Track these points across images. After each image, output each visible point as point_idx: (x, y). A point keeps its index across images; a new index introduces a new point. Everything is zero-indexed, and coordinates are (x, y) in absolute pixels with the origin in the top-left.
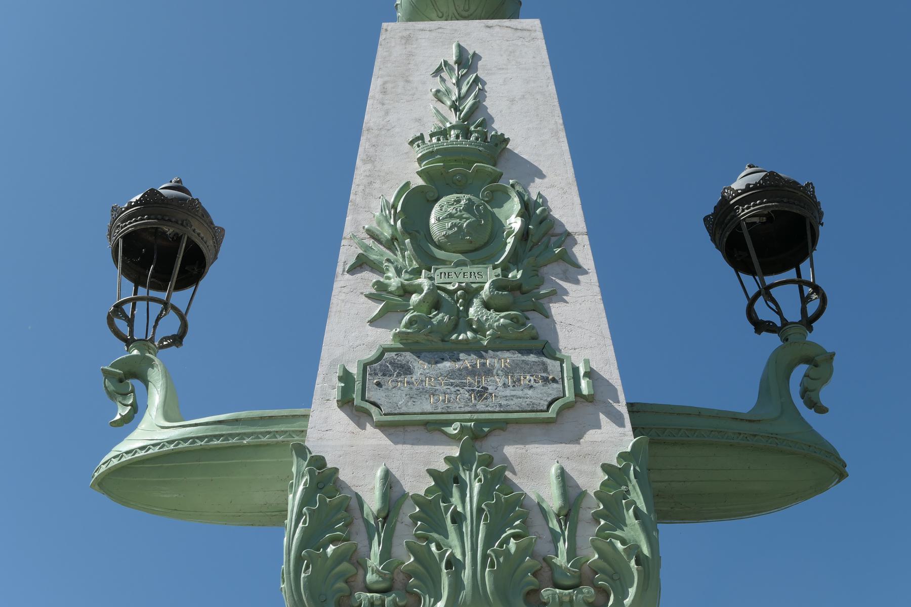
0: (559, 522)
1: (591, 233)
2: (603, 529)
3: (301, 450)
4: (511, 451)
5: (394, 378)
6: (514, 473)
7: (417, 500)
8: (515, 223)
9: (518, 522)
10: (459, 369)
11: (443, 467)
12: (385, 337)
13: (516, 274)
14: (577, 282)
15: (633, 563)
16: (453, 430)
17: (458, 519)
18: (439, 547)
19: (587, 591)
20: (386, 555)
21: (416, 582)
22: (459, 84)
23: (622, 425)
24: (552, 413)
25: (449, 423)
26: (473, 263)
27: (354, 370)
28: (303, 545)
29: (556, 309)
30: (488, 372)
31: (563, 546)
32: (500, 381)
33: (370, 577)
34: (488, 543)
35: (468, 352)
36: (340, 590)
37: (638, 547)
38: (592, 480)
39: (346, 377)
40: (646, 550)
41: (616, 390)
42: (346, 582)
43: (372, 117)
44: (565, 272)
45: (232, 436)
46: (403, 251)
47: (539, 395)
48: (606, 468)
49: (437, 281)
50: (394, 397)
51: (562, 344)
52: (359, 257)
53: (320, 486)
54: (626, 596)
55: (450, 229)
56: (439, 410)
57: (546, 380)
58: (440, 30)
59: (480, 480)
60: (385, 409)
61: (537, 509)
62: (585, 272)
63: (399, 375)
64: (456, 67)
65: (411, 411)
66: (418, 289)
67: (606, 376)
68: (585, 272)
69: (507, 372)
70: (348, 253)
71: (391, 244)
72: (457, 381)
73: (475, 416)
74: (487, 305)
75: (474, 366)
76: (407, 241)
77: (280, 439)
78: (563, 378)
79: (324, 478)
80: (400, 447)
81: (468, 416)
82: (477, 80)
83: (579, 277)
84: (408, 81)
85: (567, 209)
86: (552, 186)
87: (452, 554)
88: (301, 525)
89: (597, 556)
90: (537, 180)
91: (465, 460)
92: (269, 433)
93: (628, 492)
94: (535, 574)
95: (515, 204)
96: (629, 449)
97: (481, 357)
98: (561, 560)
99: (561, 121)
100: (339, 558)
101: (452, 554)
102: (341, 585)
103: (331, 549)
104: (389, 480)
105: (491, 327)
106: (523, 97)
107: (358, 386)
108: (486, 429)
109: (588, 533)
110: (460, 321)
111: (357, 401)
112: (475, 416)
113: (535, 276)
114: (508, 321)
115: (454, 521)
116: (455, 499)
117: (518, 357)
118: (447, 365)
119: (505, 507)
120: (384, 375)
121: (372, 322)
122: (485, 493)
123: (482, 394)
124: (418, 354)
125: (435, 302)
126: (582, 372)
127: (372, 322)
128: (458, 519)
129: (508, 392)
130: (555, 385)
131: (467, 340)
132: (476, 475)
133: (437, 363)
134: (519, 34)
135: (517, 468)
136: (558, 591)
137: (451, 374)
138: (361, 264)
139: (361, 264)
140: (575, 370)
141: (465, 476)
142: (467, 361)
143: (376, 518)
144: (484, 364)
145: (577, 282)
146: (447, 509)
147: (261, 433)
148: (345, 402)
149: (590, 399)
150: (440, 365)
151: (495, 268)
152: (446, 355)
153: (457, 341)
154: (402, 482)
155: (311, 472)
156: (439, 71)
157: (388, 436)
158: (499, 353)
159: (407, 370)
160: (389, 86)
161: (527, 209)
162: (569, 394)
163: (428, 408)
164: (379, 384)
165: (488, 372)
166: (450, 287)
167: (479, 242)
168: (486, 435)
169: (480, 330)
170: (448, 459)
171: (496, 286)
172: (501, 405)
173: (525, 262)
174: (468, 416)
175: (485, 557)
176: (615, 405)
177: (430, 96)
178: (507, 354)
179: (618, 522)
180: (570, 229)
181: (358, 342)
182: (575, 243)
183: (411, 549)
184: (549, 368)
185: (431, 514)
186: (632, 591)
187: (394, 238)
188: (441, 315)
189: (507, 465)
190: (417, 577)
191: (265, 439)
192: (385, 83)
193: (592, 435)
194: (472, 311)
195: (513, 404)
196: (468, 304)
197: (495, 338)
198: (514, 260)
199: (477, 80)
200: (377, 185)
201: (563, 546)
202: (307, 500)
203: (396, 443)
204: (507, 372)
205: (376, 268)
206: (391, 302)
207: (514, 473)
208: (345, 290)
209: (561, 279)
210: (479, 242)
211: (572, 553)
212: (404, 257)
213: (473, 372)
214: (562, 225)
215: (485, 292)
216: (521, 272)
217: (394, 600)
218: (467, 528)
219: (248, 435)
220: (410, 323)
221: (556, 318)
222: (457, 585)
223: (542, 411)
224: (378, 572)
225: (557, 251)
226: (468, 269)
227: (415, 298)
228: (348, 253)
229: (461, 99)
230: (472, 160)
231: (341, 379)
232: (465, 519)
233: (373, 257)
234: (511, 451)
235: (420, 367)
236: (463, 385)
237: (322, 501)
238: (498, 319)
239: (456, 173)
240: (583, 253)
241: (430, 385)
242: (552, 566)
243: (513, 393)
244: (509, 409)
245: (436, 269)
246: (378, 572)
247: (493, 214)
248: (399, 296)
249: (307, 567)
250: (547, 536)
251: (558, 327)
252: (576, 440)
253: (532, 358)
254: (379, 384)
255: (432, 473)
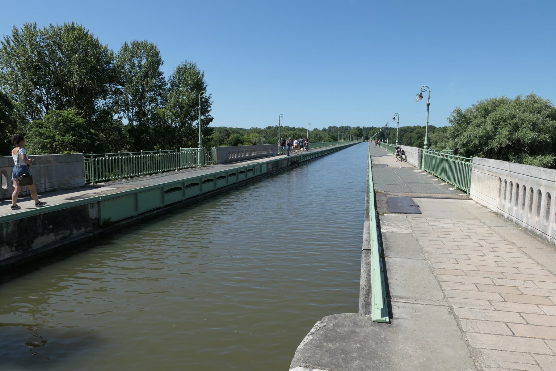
4: (101, 223)
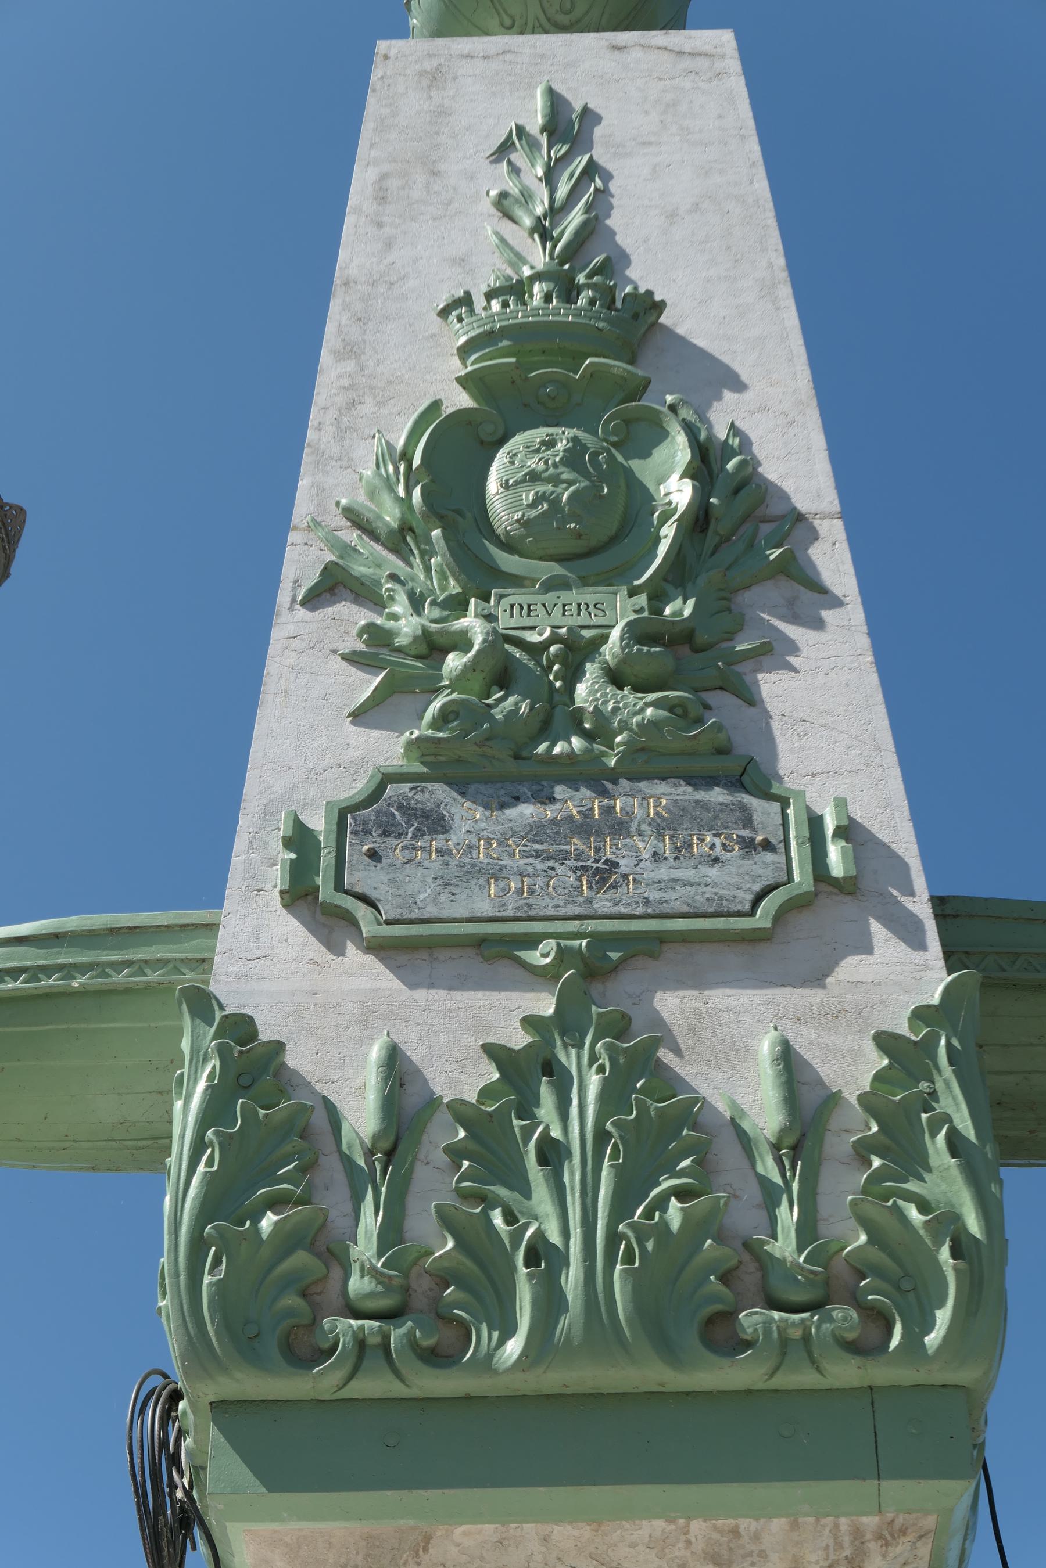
0: (779, 1161)
1: (850, 513)
2: (877, 1177)
3: (201, 1003)
4: (670, 1004)
5: (407, 840)
6: (678, 1052)
7: (460, 1112)
8: (679, 492)
9: (686, 1163)
10: (554, 821)
11: (518, 1039)
12: (388, 748)
13: (681, 608)
14: (818, 624)
15: (945, 1254)
16: (540, 956)
17: (551, 1154)
18: (510, 1218)
19: (843, 1315)
20: (391, 1234)
21: (461, 1295)
22: (550, 178)
23: (920, 945)
24: (762, 919)
25: (532, 941)
26: (585, 582)
27: (318, 822)
28: (206, 1212)
29: (770, 685)
30: (620, 827)
31: (788, 1216)
32: (645, 848)
33: (357, 1285)
34: (621, 1208)
35: (573, 782)
36: (290, 1312)
37: (956, 1218)
38: (852, 1069)
39: (300, 839)
40: (974, 1225)
41: (905, 867)
42: (304, 1294)
43: (354, 255)
44: (791, 602)
45: (47, 970)
46: (426, 555)
47: (733, 877)
48: (885, 1041)
49: (504, 623)
50: (409, 883)
51: (784, 765)
52: (328, 570)
53: (245, 1081)
54: (928, 1326)
55: (533, 505)
56: (510, 913)
57: (749, 845)
58: (508, 57)
59: (601, 1069)
60: (387, 911)
61: (729, 1133)
62: (837, 603)
63: (418, 834)
64: (544, 140)
65: (446, 914)
66: (461, 642)
67: (885, 836)
68: (837, 603)
69: (661, 827)
70: (302, 562)
71: (400, 540)
72: (552, 848)
73: (591, 926)
74: (615, 678)
75: (587, 813)
76: (436, 533)
77: (154, 977)
78: (786, 841)
79: (252, 1066)
80: (421, 994)
81: (573, 926)
82: (592, 169)
83: (825, 614)
84: (435, 173)
85: (797, 463)
86: (763, 409)
87: (540, 1234)
88: (201, 1168)
89: (863, 1238)
90: (728, 396)
91: (567, 1024)
92: (129, 963)
93: (933, 1094)
94: (725, 1278)
95: (678, 450)
96: (936, 1000)
97: (603, 793)
98: (784, 1246)
99: (781, 261)
100: (288, 1240)
101: (540, 1234)
102: (291, 1300)
103: (268, 1222)
104: (397, 1069)
105: (624, 726)
106: (696, 208)
107: (326, 860)
108: (615, 956)
109: (844, 1187)
110: (555, 714)
111: (326, 892)
112: (591, 926)
113: (723, 609)
114: (663, 713)
115: (543, 1160)
116: (547, 1110)
117: (685, 793)
118: (527, 811)
119: (660, 1125)
120: (386, 834)
121: (359, 716)
122: (613, 1096)
123: (605, 875)
124: (461, 786)
125: (499, 671)
126: (830, 825)
127: (359, 716)
128: (551, 1154)
129: (663, 872)
130: (769, 857)
131: (570, 757)
132: (593, 1058)
133: (503, 806)
134: (687, 63)
135: (684, 1042)
136: (776, 1315)
137: (536, 831)
138: (332, 586)
139: (332, 586)
140: (815, 822)
141: (569, 1059)
142: (571, 801)
143: (369, 1153)
144: (609, 810)
145: (818, 624)
146: (527, 1133)
147: (112, 965)
148: (299, 895)
149: (847, 887)
150: (511, 813)
151: (633, 593)
152: (525, 790)
153: (549, 759)
154: (428, 1074)
155: (223, 1052)
156: (504, 149)
157: (396, 969)
158: (643, 785)
159: (436, 823)
160: (393, 183)
161: (705, 463)
162: (801, 875)
163: (485, 908)
164: (373, 855)
165: (620, 827)
166: (534, 637)
167: (597, 535)
168: (615, 968)
169: (600, 732)
170: (530, 1022)
171: (636, 633)
172: (647, 902)
173: (702, 581)
174: (573, 926)
175: (613, 1238)
176: (905, 901)
177: (487, 206)
178: (661, 788)
179: (909, 1160)
180: (802, 504)
181: (328, 761)
182: (814, 536)
183: (447, 1221)
184: (757, 818)
185: (492, 1144)
186: (943, 1317)
187: (405, 528)
188: (512, 699)
189: (658, 1021)
190: (463, 1284)
191: (120, 978)
192: (383, 177)
193: (851, 968)
194: (582, 689)
195: (676, 899)
196: (573, 675)
197: (633, 750)
198: (677, 575)
199: (592, 169)
200: (367, 407)
201: (788, 1216)
202: (215, 1111)
203: (412, 986)
204: (661, 827)
205: (366, 594)
206: (400, 672)
207: (678, 1052)
208: (296, 644)
209: (783, 618)
210: (597, 535)
211: (807, 1231)
212: (428, 569)
213: (584, 827)
214: (784, 496)
215: (612, 648)
216: (691, 602)
217: (410, 1334)
218: (572, 1175)
219: (82, 969)
220: (444, 718)
221: (773, 706)
222: (551, 1303)
223: (740, 914)
224: (373, 1272)
225: (774, 554)
226: (572, 596)
227: (454, 662)
228: (302, 562)
229: (556, 212)
230: (582, 350)
231: (288, 843)
232: (569, 1154)
233: (359, 569)
234: (670, 1004)
235: (467, 817)
236: (562, 857)
237: (249, 1116)
238: (641, 708)
239: (544, 381)
240: (832, 559)
241: (487, 856)
242: (763, 1262)
243: (676, 874)
244: (665, 909)
245: (501, 597)
246: (373, 1272)
247: (629, 473)
248: (419, 657)
249: (217, 1262)
250: (752, 1192)
251: (775, 726)
252: (817, 978)
253: (718, 795)
254: (373, 855)
255: (495, 1052)
